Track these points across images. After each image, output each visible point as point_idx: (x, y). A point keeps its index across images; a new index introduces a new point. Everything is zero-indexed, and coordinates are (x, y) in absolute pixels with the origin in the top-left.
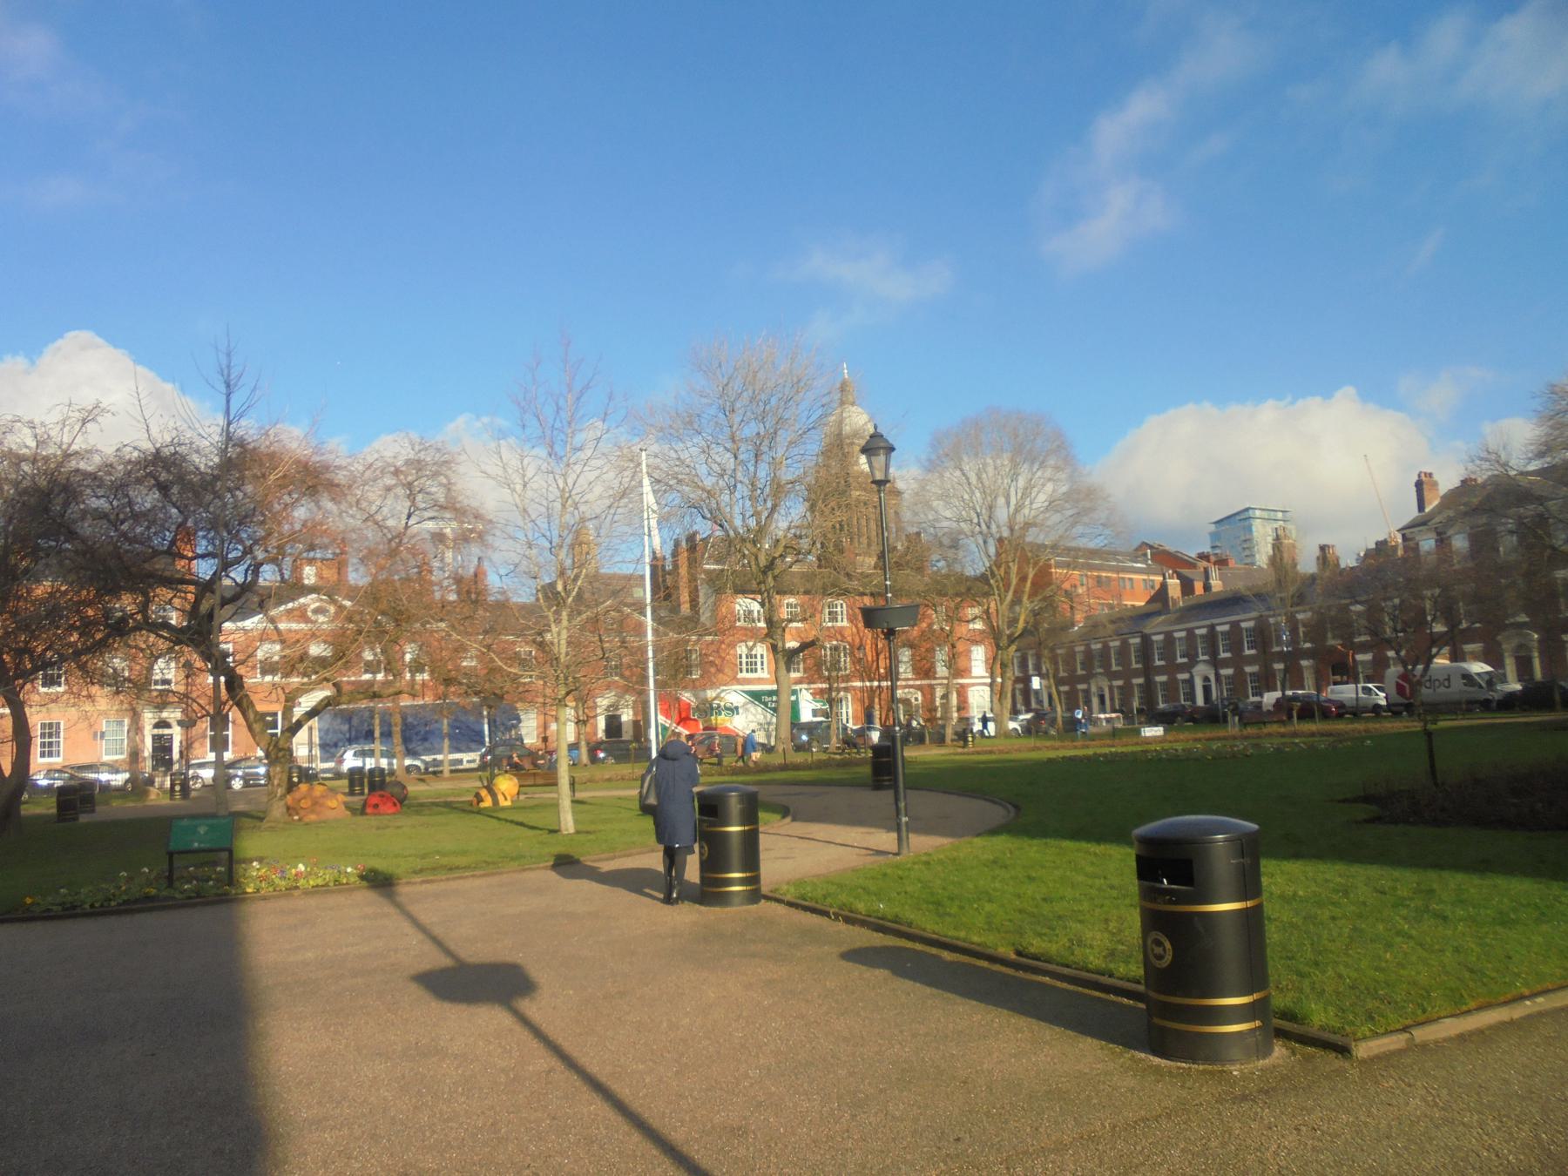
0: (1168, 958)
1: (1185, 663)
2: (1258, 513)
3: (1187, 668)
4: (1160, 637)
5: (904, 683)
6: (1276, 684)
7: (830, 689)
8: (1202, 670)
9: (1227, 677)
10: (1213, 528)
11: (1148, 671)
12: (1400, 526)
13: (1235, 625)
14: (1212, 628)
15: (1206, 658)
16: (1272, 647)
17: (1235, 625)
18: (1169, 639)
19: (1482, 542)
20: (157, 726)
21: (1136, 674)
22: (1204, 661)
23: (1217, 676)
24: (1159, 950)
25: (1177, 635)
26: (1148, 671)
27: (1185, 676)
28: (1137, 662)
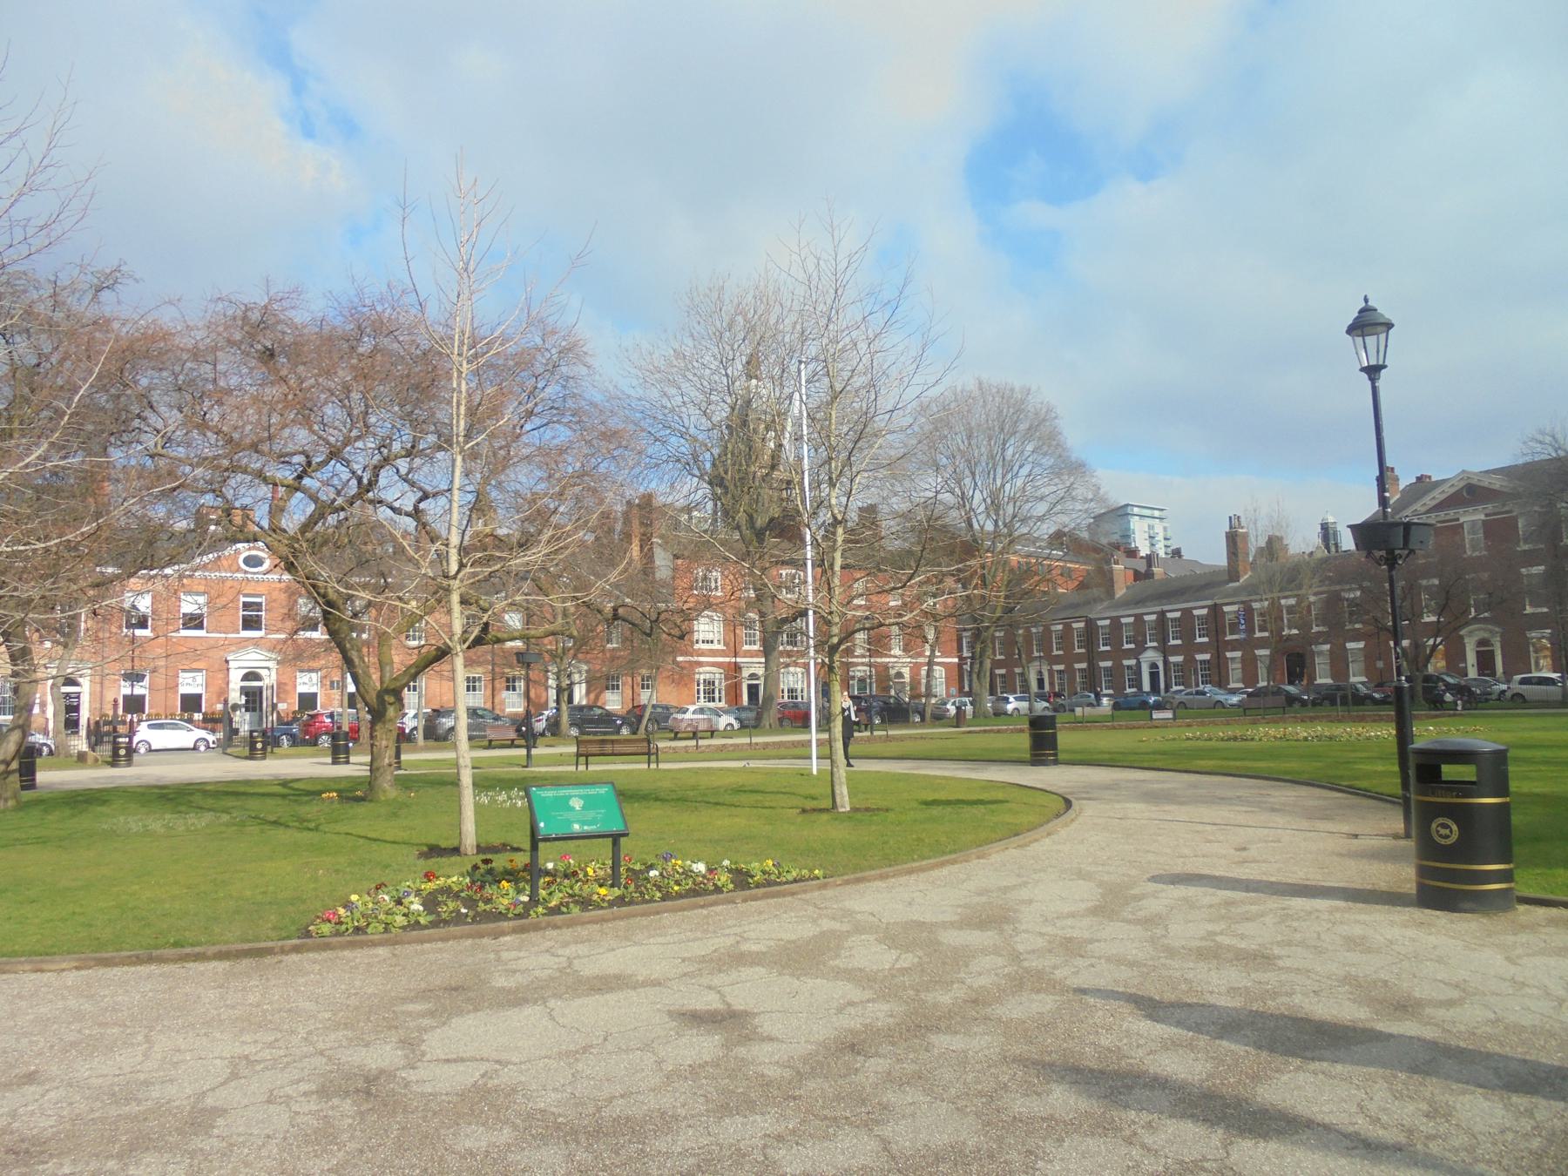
1: (1107, 651)
2: (1136, 510)
3: (1136, 654)
4: (1154, 617)
8: (1150, 656)
9: (1176, 664)
11: (1092, 657)
13: (1187, 612)
14: (1162, 614)
15: (1155, 644)
16: (1225, 635)
17: (1187, 612)
18: (1116, 623)
20: (246, 677)
21: (1079, 658)
22: (1154, 647)
23: (1166, 662)
25: (1124, 620)
26: (1092, 657)
27: (1133, 662)
28: (1001, 654)
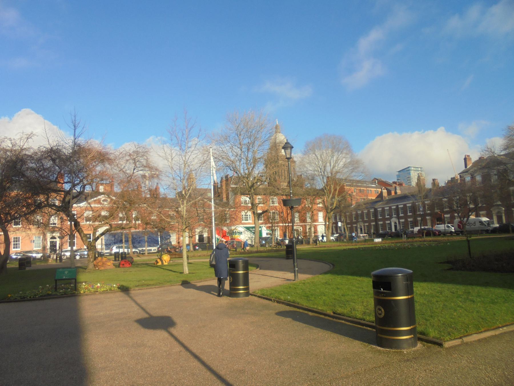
0: (383, 314)
1: (388, 218)
2: (412, 168)
3: (389, 219)
4: (380, 209)
5: (296, 224)
6: (418, 225)
7: (272, 226)
8: (394, 220)
9: (402, 222)
10: (398, 173)
11: (376, 220)
12: (459, 173)
13: (405, 205)
14: (397, 206)
15: (395, 216)
16: (417, 213)
17: (405, 205)
18: (383, 210)
19: (486, 178)
20: (51, 238)
21: (372, 221)
22: (395, 217)
23: (399, 222)
24: (380, 312)
25: (386, 208)
26: (376, 220)
27: (389, 222)
28: (373, 217)
